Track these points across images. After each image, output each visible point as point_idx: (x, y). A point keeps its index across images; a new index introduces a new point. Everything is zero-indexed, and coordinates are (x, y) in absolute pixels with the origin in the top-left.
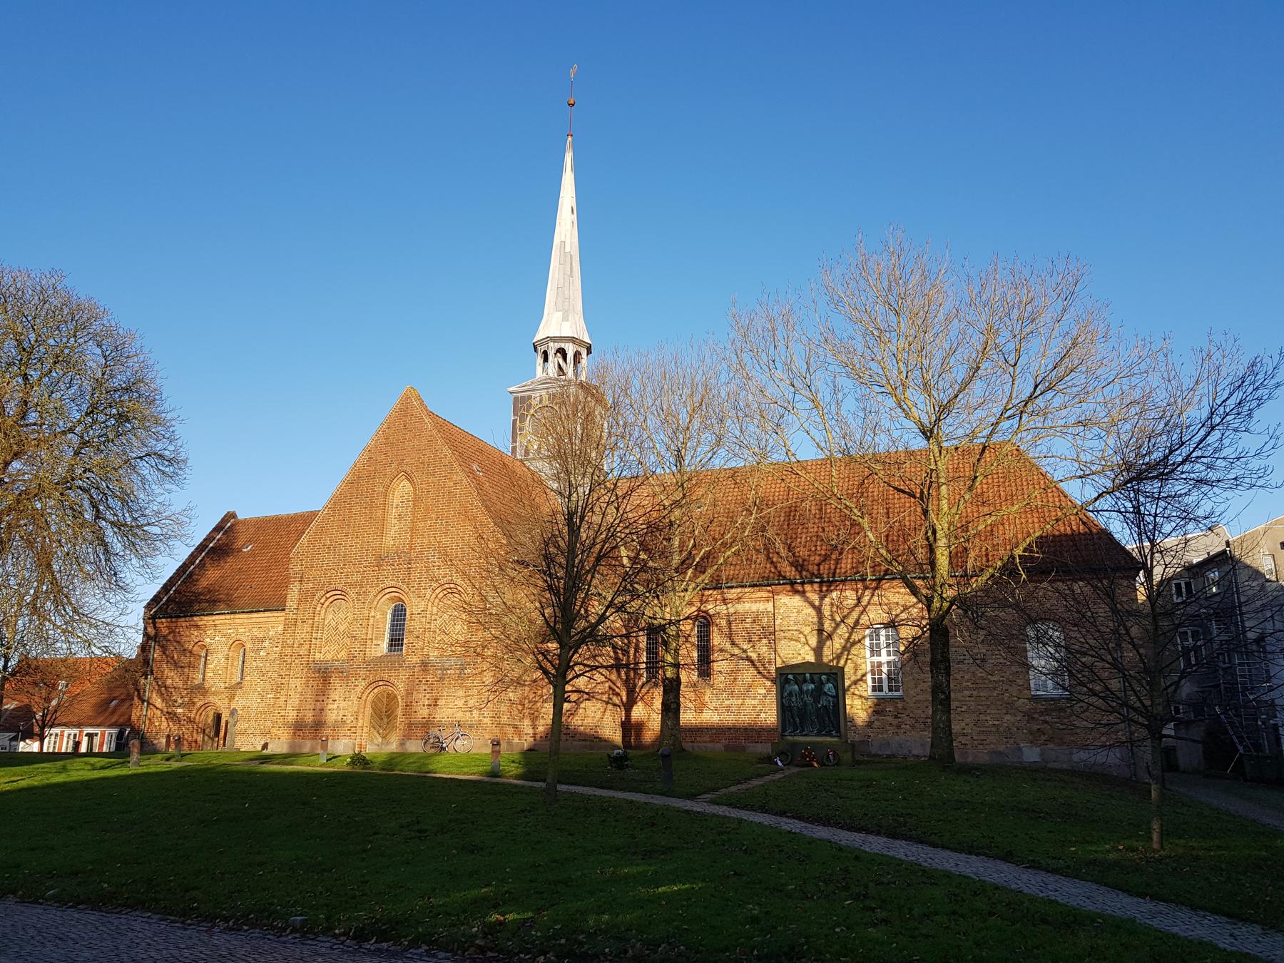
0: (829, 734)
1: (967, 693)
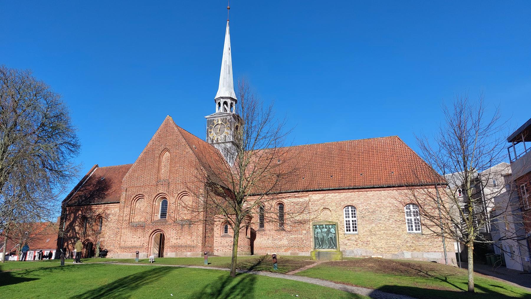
0: (332, 248)
1: (383, 232)
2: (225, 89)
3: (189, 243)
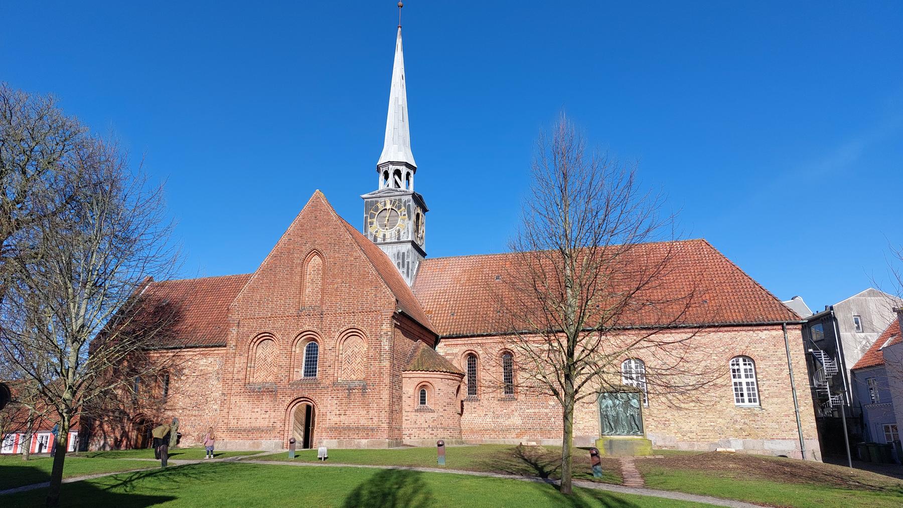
0: (635, 434)
2: (396, 147)
3: (363, 422)
